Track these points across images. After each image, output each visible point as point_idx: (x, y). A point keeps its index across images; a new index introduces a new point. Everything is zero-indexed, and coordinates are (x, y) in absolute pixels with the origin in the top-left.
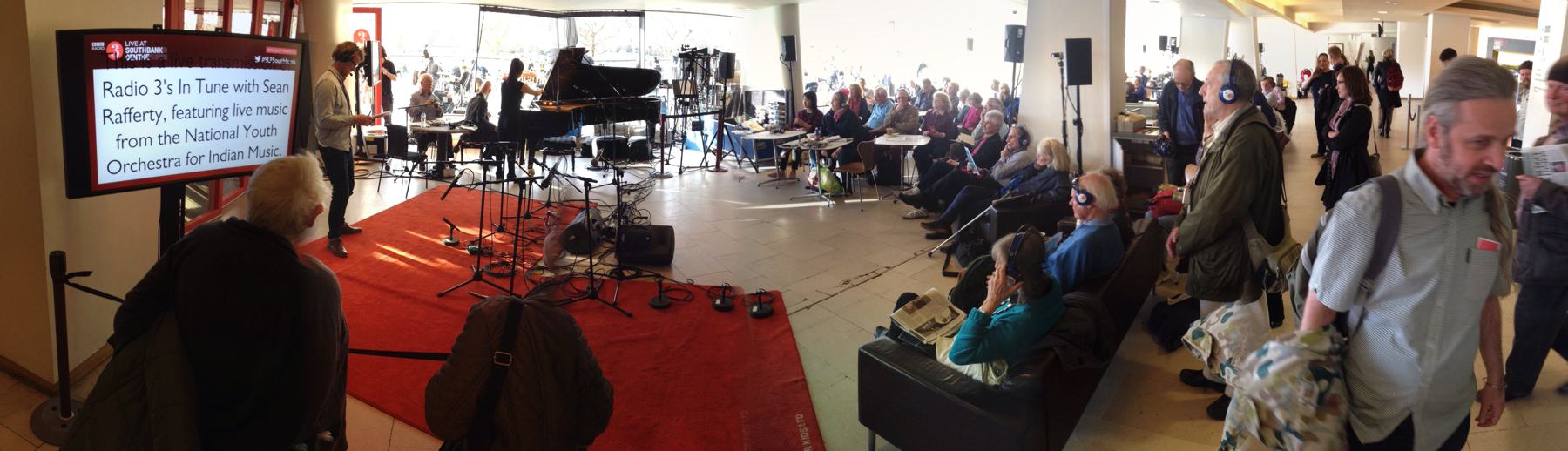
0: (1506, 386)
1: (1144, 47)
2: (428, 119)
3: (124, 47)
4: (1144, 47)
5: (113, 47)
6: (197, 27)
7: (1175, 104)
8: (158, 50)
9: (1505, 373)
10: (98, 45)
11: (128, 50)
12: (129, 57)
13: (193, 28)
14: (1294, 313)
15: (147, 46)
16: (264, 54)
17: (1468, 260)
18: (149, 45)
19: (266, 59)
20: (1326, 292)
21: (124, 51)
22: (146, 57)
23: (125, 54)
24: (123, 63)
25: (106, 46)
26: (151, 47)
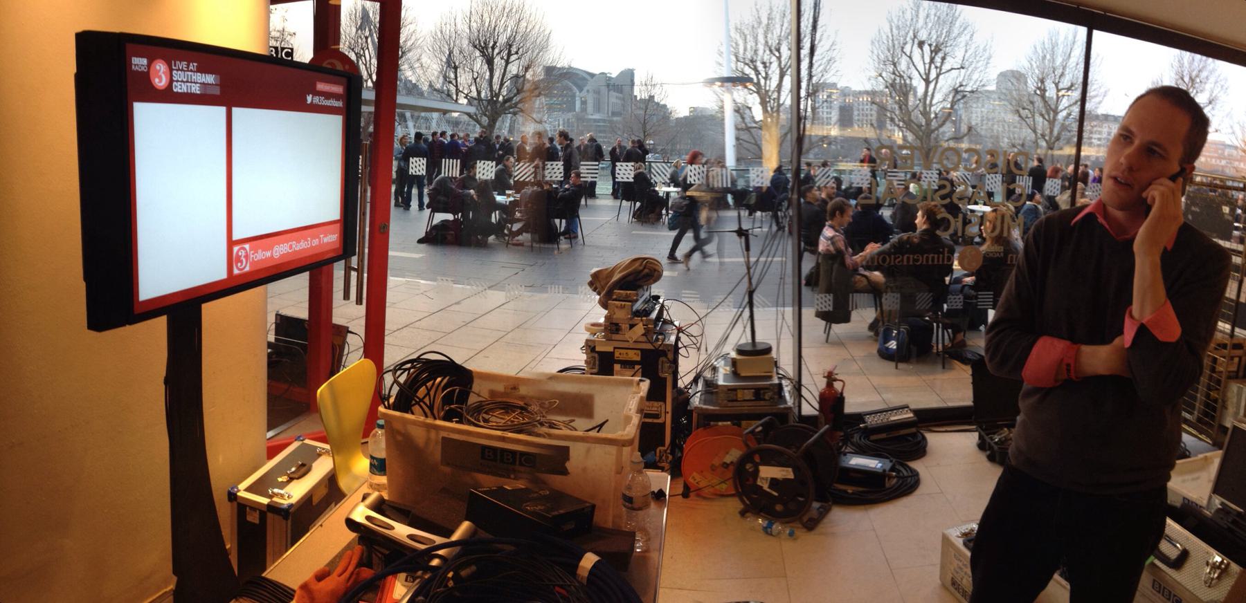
0: (446, 142)
1: (1126, 95)
2: (457, 186)
3: (171, 70)
4: (1126, 95)
5: (158, 67)
6: (365, 100)
7: (297, 476)
8: (210, 79)
9: (729, 423)
10: (139, 63)
11: (177, 75)
12: (179, 88)
13: (362, 110)
14: (730, 336)
15: (197, 71)
16: (317, 93)
17: (488, 357)
18: (200, 70)
19: (317, 100)
20: (779, 34)
21: (171, 76)
22: (196, 89)
23: (171, 81)
24: (167, 96)
25: (149, 65)
26: (201, 73)
